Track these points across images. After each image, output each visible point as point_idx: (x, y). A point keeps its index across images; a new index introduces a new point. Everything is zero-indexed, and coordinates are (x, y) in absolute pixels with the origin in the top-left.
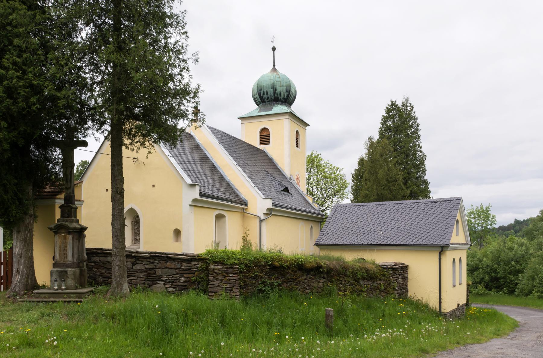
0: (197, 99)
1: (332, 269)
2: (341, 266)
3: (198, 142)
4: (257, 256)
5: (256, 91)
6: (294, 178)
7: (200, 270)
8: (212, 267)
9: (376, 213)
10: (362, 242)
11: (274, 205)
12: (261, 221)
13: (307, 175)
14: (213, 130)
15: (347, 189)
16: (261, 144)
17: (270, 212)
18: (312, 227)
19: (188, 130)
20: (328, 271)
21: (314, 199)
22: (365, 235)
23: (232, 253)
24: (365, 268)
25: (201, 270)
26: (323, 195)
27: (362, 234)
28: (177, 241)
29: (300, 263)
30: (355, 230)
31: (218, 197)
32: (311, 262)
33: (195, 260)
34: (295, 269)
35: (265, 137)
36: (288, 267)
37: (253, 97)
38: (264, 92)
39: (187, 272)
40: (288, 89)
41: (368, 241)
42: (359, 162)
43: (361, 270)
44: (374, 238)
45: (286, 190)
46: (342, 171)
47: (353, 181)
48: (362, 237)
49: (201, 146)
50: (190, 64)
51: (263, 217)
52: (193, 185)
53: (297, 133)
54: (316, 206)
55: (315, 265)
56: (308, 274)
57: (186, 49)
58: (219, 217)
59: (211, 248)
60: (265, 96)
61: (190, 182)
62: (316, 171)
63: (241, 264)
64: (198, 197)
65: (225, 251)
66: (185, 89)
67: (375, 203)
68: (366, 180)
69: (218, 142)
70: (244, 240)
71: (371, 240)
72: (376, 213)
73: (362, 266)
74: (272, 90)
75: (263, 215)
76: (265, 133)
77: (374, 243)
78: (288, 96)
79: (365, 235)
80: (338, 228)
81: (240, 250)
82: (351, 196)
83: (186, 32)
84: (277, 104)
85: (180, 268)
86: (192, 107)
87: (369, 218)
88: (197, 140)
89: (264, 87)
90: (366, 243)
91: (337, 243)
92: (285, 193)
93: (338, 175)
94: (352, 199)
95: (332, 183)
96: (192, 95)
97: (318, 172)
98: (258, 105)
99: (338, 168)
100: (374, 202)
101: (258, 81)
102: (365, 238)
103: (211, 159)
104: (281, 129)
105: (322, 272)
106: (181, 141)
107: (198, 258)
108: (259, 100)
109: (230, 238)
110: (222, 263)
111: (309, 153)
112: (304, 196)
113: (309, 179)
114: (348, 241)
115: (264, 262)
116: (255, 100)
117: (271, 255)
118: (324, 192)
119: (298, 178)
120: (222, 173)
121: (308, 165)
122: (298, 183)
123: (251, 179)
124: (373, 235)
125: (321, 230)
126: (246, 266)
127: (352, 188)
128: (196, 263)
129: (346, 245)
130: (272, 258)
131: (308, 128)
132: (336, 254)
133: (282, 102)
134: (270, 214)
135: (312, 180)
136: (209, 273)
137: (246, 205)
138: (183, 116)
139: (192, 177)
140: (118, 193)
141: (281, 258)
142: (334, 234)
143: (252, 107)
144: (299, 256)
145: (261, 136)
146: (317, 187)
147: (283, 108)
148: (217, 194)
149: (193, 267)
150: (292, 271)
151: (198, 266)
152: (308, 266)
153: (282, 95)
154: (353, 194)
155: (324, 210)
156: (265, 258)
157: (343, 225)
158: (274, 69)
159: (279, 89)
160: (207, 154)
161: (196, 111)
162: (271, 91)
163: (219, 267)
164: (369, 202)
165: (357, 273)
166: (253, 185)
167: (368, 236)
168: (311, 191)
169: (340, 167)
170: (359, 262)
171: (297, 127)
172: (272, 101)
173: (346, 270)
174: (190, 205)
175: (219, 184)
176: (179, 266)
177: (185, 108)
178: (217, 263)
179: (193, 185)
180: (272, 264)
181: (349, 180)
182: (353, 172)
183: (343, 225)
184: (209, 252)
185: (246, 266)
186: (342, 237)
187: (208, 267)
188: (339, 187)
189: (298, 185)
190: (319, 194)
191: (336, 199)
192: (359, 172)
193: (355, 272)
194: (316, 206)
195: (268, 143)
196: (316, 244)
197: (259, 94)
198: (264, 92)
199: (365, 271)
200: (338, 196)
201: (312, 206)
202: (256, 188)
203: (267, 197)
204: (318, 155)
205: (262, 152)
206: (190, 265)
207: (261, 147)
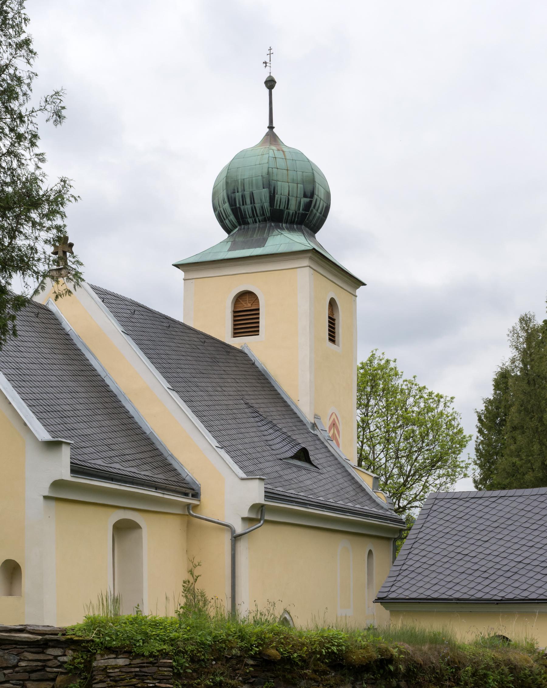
0: (58, 221)
1: (420, 667)
2: (443, 658)
3: (68, 329)
4: (222, 633)
5: (223, 194)
6: (325, 423)
7: (70, 671)
8: (100, 662)
9: (538, 517)
10: (502, 594)
11: (269, 495)
12: (236, 538)
13: (358, 415)
14: (107, 297)
15: (465, 451)
16: (236, 333)
17: (258, 515)
18: (370, 552)
19: (39, 299)
20: (408, 670)
21: (376, 479)
22: (509, 574)
23: (156, 624)
24: (508, 663)
25: (73, 671)
26: (401, 468)
27: (500, 573)
28: (10, 593)
29: (334, 649)
30: (483, 562)
31: (119, 474)
32: (365, 648)
33: (57, 644)
34: (323, 667)
35: (246, 315)
36: (303, 660)
37: (215, 209)
38: (243, 197)
39: (34, 676)
40: (309, 188)
41: (517, 592)
42: (496, 380)
43: (498, 666)
44: (531, 581)
45: (303, 455)
46: (452, 405)
47: (480, 431)
48: (501, 580)
49: (76, 341)
50: (40, 122)
51: (239, 528)
52: (53, 445)
53: (332, 304)
54: (382, 498)
55: (376, 656)
56: (356, 680)
57: (29, 85)
58: (124, 529)
59: (99, 613)
60: (248, 207)
61: (44, 435)
62: (383, 403)
63: (177, 654)
64: (66, 475)
65: (135, 619)
66: (29, 194)
67: (536, 490)
68: (514, 428)
69: (120, 329)
70: (188, 589)
71: (524, 587)
72: (538, 517)
73: (500, 657)
74: (265, 192)
75: (240, 522)
76: (247, 305)
77: (534, 596)
78: (308, 206)
79: (509, 574)
80: (437, 558)
81: (175, 616)
82: (475, 471)
83: (27, 42)
84: (278, 227)
85: (17, 666)
86: (46, 242)
87: (520, 529)
88: (64, 325)
89: (243, 185)
90: (511, 596)
91: (435, 596)
92: (299, 463)
93: (441, 414)
94: (478, 478)
95: (423, 436)
96: (46, 208)
97: (387, 407)
98: (228, 231)
99: (440, 397)
100: (534, 486)
101: (229, 168)
102: (509, 582)
103: (103, 375)
104: (289, 298)
105: (395, 674)
106: (15, 334)
107: (63, 638)
108: (232, 217)
109: (156, 584)
110: (129, 652)
111: (362, 357)
112: (350, 470)
113: (364, 425)
114: (465, 590)
115: (241, 649)
116: (221, 218)
117: (258, 629)
118: (403, 461)
119: (334, 425)
120: (132, 412)
121: (361, 390)
122: (334, 438)
123: (210, 428)
124: (531, 574)
125: (394, 558)
126: (193, 660)
127: (477, 450)
128: (57, 652)
129: (459, 601)
130: (260, 637)
131: (360, 291)
132: (429, 625)
133: (292, 222)
134: (259, 521)
135: (372, 429)
136: (92, 678)
137: (196, 495)
138: (23, 263)
139: (52, 421)
140: (87, 291)
141: (285, 638)
142: (426, 573)
143: (212, 236)
144: (333, 632)
145: (236, 314)
146: (386, 449)
147: (295, 240)
148: (117, 467)
149: (50, 664)
150: (315, 671)
151: (65, 659)
152: (357, 657)
153: (293, 206)
154: (481, 466)
155: (404, 508)
156: (242, 638)
157: (451, 548)
158: (271, 136)
159: (283, 189)
160: (93, 362)
161: (63, 245)
162: (262, 195)
163: (121, 662)
164: (521, 487)
165: (485, 676)
166: (214, 443)
167: (516, 577)
168: (371, 457)
169: (446, 391)
170: (493, 647)
171: (332, 290)
172: (265, 220)
173: (458, 669)
174: (46, 498)
175: (123, 440)
176: (13, 660)
177: (27, 242)
178: (115, 651)
179: (53, 445)
180: (260, 653)
181: (470, 427)
182: (481, 407)
183: (451, 548)
184: (93, 624)
185: (193, 660)
186: (449, 579)
187: (90, 662)
188: (442, 447)
189: (333, 443)
190: (390, 464)
191: (435, 480)
192: (497, 408)
193: (481, 672)
194: (382, 498)
195: (254, 330)
196: (380, 600)
197: (232, 202)
198: (243, 197)
199: (506, 670)
200: (442, 472)
201: (370, 498)
202: (222, 452)
203: (250, 475)
204: (388, 361)
205: (241, 358)
206: (41, 657)
207: (237, 343)
